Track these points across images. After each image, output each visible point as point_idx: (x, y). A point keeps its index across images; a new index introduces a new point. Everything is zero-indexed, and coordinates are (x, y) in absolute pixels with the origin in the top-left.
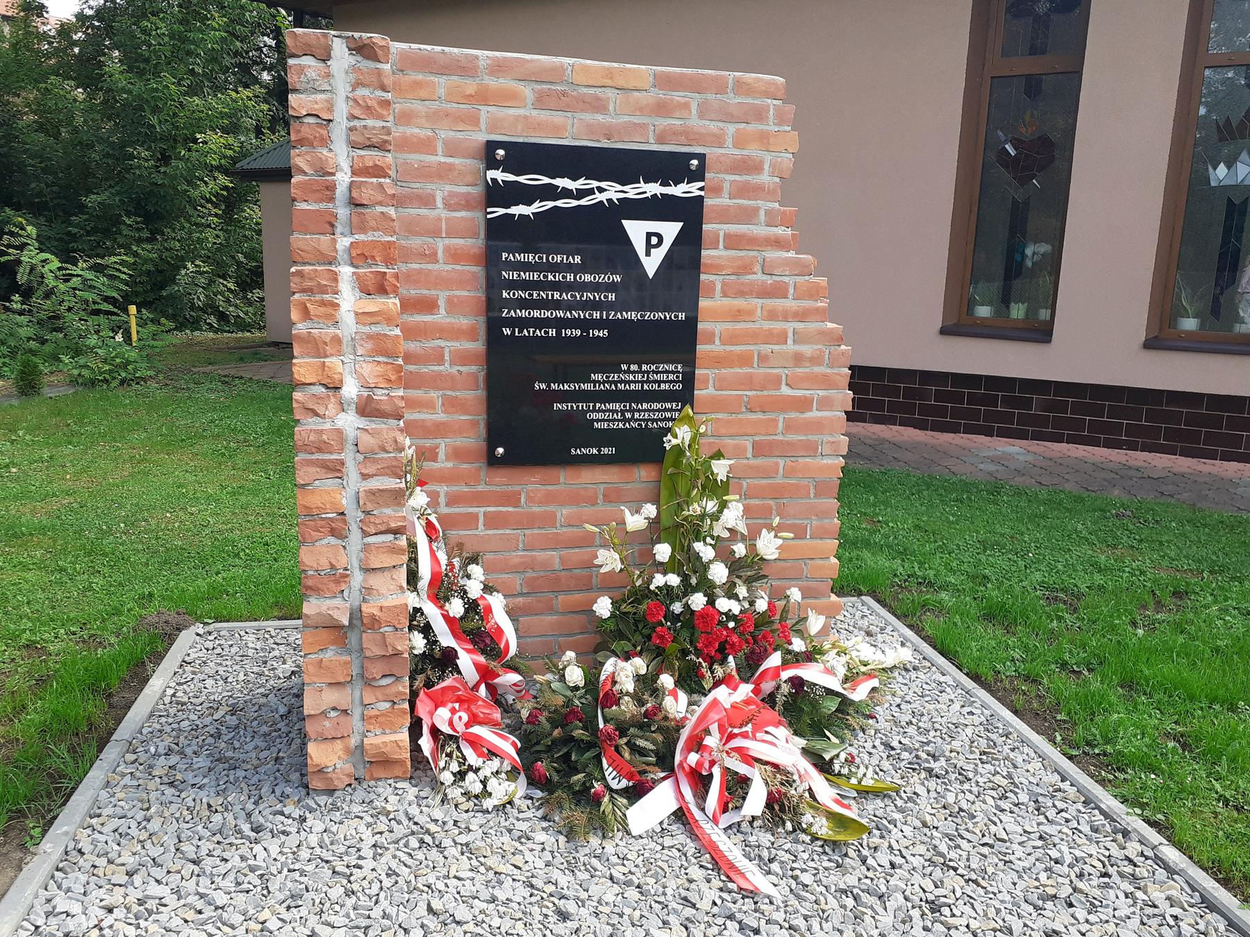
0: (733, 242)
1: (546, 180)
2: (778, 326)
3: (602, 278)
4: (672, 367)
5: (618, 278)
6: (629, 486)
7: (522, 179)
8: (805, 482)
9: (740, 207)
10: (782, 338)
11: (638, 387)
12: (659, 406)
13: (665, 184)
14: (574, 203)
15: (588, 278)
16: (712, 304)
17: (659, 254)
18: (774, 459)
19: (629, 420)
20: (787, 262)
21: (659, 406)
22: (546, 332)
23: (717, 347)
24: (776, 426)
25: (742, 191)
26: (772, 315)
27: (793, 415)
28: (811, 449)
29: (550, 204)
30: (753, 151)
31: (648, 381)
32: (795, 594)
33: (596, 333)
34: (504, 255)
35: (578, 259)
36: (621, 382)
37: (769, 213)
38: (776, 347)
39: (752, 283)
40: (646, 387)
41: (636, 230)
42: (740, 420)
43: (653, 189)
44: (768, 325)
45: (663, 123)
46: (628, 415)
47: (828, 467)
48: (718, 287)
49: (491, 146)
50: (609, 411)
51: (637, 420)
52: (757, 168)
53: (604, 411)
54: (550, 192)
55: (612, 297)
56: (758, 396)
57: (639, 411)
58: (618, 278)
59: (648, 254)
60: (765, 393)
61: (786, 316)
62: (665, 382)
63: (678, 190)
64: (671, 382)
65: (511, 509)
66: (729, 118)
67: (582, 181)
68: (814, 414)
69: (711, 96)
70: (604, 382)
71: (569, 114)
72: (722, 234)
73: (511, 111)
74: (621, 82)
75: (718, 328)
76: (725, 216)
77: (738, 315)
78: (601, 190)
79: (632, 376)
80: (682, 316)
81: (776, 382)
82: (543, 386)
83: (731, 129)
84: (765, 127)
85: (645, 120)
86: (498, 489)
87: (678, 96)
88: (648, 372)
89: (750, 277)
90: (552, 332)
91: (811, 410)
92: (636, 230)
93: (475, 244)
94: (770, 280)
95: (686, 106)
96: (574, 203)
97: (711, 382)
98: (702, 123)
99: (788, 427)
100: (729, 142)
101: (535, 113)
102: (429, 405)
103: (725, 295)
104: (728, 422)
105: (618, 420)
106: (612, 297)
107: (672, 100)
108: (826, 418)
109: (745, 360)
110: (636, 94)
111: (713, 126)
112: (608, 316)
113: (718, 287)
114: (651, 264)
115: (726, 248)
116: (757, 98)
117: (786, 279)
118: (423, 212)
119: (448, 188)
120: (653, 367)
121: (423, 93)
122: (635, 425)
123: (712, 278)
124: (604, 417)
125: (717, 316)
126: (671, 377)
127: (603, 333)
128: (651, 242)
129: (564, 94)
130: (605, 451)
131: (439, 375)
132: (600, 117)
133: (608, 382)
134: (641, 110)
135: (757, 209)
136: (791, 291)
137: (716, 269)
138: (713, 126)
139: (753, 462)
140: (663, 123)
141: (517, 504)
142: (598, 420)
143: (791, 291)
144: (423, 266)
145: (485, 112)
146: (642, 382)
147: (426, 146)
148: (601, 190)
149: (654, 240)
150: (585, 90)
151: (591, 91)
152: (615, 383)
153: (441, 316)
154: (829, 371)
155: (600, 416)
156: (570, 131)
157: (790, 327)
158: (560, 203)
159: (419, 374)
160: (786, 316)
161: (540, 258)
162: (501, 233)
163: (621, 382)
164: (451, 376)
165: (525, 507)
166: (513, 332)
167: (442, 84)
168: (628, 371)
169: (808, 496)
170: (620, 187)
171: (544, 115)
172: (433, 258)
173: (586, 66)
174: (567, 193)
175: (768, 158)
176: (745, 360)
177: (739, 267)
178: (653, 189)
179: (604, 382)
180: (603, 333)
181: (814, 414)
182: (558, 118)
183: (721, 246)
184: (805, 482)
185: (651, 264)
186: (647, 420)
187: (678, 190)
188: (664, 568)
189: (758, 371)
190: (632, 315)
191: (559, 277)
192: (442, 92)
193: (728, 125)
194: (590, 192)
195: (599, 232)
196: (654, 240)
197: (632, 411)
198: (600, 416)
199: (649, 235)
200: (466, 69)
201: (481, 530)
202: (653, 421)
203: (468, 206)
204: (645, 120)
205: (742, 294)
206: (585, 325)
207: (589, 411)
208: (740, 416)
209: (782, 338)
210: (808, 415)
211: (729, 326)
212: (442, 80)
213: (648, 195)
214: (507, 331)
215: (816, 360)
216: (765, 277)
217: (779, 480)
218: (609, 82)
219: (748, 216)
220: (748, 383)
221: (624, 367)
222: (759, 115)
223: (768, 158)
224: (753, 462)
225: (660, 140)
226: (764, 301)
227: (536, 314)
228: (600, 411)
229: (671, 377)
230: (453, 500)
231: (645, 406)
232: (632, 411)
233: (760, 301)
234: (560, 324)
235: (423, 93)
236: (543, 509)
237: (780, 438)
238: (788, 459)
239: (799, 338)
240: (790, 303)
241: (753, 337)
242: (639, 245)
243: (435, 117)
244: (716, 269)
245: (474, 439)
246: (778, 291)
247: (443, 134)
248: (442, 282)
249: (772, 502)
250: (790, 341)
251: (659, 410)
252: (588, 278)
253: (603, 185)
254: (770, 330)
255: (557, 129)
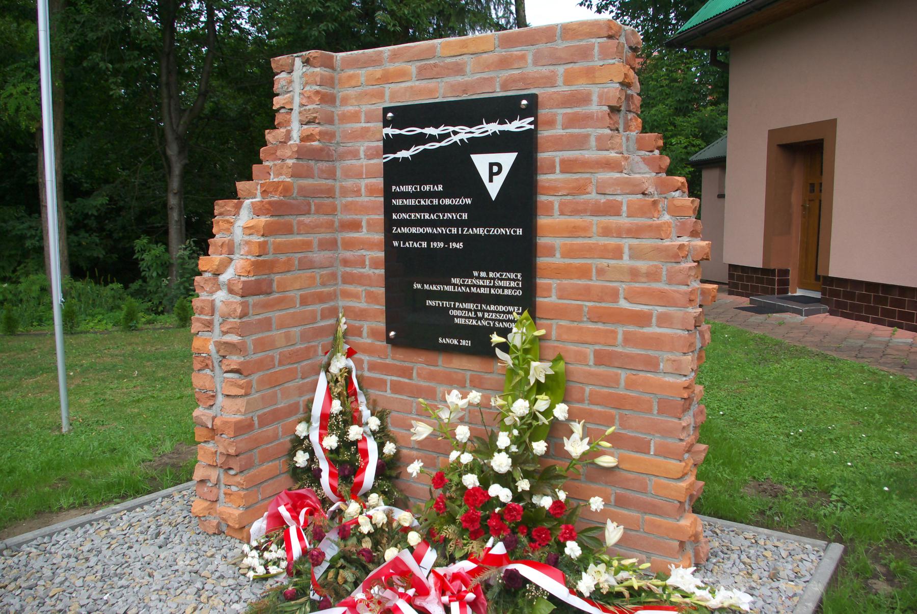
0: (568, 166)
1: (419, 130)
2: (612, 241)
3: (457, 202)
4: (513, 276)
5: (469, 201)
6: (489, 376)
7: (403, 132)
8: (647, 396)
9: (572, 135)
10: (617, 253)
11: (487, 291)
12: (504, 309)
13: (502, 123)
14: (437, 145)
15: (447, 202)
16: (551, 221)
17: (499, 180)
18: (615, 370)
19: (480, 319)
20: (618, 183)
21: (504, 309)
22: (421, 245)
23: (557, 260)
24: (615, 338)
25: (572, 121)
26: (606, 232)
27: (631, 328)
28: (652, 365)
29: (421, 148)
30: (581, 86)
31: (494, 287)
32: (596, 503)
33: (454, 245)
34: (394, 188)
35: (440, 188)
36: (474, 286)
37: (599, 138)
38: (612, 262)
39: (586, 202)
40: (492, 291)
41: (481, 162)
42: (581, 329)
43: (493, 128)
44: (604, 241)
45: (505, 74)
46: (480, 314)
47: (671, 386)
48: (556, 206)
49: (386, 110)
50: (465, 309)
51: (486, 319)
52: (585, 99)
53: (461, 309)
54: (421, 139)
55: (465, 216)
56: (596, 307)
57: (488, 311)
58: (469, 201)
59: (491, 180)
60: (603, 305)
61: (620, 232)
62: (508, 288)
63: (512, 127)
64: (512, 288)
65: (406, 380)
66: (557, 61)
67: (442, 128)
68: (653, 329)
69: (541, 46)
70: (461, 285)
71: (439, 80)
72: (557, 160)
73: (403, 85)
74: (472, 49)
75: (558, 242)
76: (559, 144)
77: (574, 231)
78: (455, 133)
79: (482, 281)
80: (520, 232)
81: (614, 295)
82: (419, 286)
83: (561, 70)
84: (591, 64)
85: (492, 74)
86: (398, 363)
87: (516, 51)
88: (494, 279)
89: (584, 197)
90: (424, 245)
91: (649, 325)
92: (481, 162)
93: (379, 182)
94: (603, 199)
95: (523, 58)
96: (437, 145)
97: (554, 291)
98: (535, 69)
99: (628, 339)
100: (560, 81)
101: (417, 83)
102: (356, 296)
103: (562, 213)
104: (569, 329)
105: (472, 318)
106: (465, 216)
107: (512, 55)
108: (665, 335)
109: (584, 272)
110: (485, 55)
111: (545, 70)
112: (463, 231)
113: (556, 206)
114: (494, 189)
115: (562, 172)
116: (582, 40)
117: (619, 198)
118: (354, 162)
119: (366, 144)
120: (498, 275)
121: (353, 83)
122: (485, 323)
123: (551, 198)
124: (462, 315)
125: (557, 231)
126: (513, 284)
127: (460, 245)
128: (493, 170)
129: (435, 65)
130: (463, 343)
131: (362, 276)
132: (459, 79)
133: (464, 285)
134: (488, 67)
135: (587, 136)
136: (624, 208)
137: (553, 190)
138: (545, 70)
139: (595, 369)
140: (505, 74)
141: (410, 377)
142: (457, 317)
143: (624, 208)
144: (354, 199)
145: (388, 88)
146: (490, 287)
147: (355, 117)
148: (455, 133)
149: (495, 169)
150: (449, 60)
151: (454, 60)
152: (469, 286)
153: (363, 234)
154: (667, 287)
155: (459, 313)
156: (441, 91)
157: (627, 243)
158: (427, 146)
159: (351, 274)
160: (620, 232)
161: (416, 188)
162: (394, 173)
163: (474, 286)
164: (369, 276)
165: (416, 381)
166: (399, 244)
167: (362, 73)
168: (479, 278)
169: (650, 411)
170: (468, 129)
171: (424, 83)
172: (358, 193)
173: (449, 42)
174: (432, 138)
175: (595, 90)
176: (584, 272)
177: (574, 188)
178: (493, 128)
179: (461, 285)
180: (460, 245)
181: (654, 329)
182: (432, 84)
183: (558, 171)
184: (647, 396)
185: (494, 189)
186: (495, 320)
187: (512, 127)
188: (462, 448)
189: (595, 282)
190: (480, 231)
191: (428, 202)
192: (363, 79)
193: (556, 67)
194: (447, 135)
195: (453, 168)
196: (495, 169)
197: (483, 311)
198: (459, 313)
199: (491, 165)
200: (376, 62)
201: (389, 393)
202: (500, 321)
203: (377, 156)
204: (492, 74)
205: (576, 212)
206: (447, 238)
207: (450, 308)
208: (581, 325)
209: (617, 253)
210: (646, 330)
211: (568, 241)
212: (362, 72)
213: (490, 133)
214: (396, 244)
215: (653, 275)
216: (599, 197)
217: (621, 391)
218: (465, 51)
219: (580, 142)
220: (586, 293)
221: (476, 274)
222: (585, 53)
223: (595, 90)
224: (595, 369)
225: (465, 92)
226: (599, 218)
227: (413, 230)
228: (458, 309)
229: (513, 284)
230: (373, 367)
231: (493, 308)
232: (483, 311)
233: (595, 218)
234: (429, 238)
235: (353, 83)
236: (427, 384)
237: (619, 349)
238: (629, 372)
239: (636, 254)
240: (623, 220)
241: (589, 252)
242: (484, 174)
243: (361, 97)
244: (553, 190)
245: (382, 325)
246: (613, 209)
247: (364, 108)
248: (365, 209)
249: (614, 411)
250: (626, 257)
251: (504, 312)
252: (447, 202)
253: (457, 129)
254: (605, 245)
255: (431, 91)
